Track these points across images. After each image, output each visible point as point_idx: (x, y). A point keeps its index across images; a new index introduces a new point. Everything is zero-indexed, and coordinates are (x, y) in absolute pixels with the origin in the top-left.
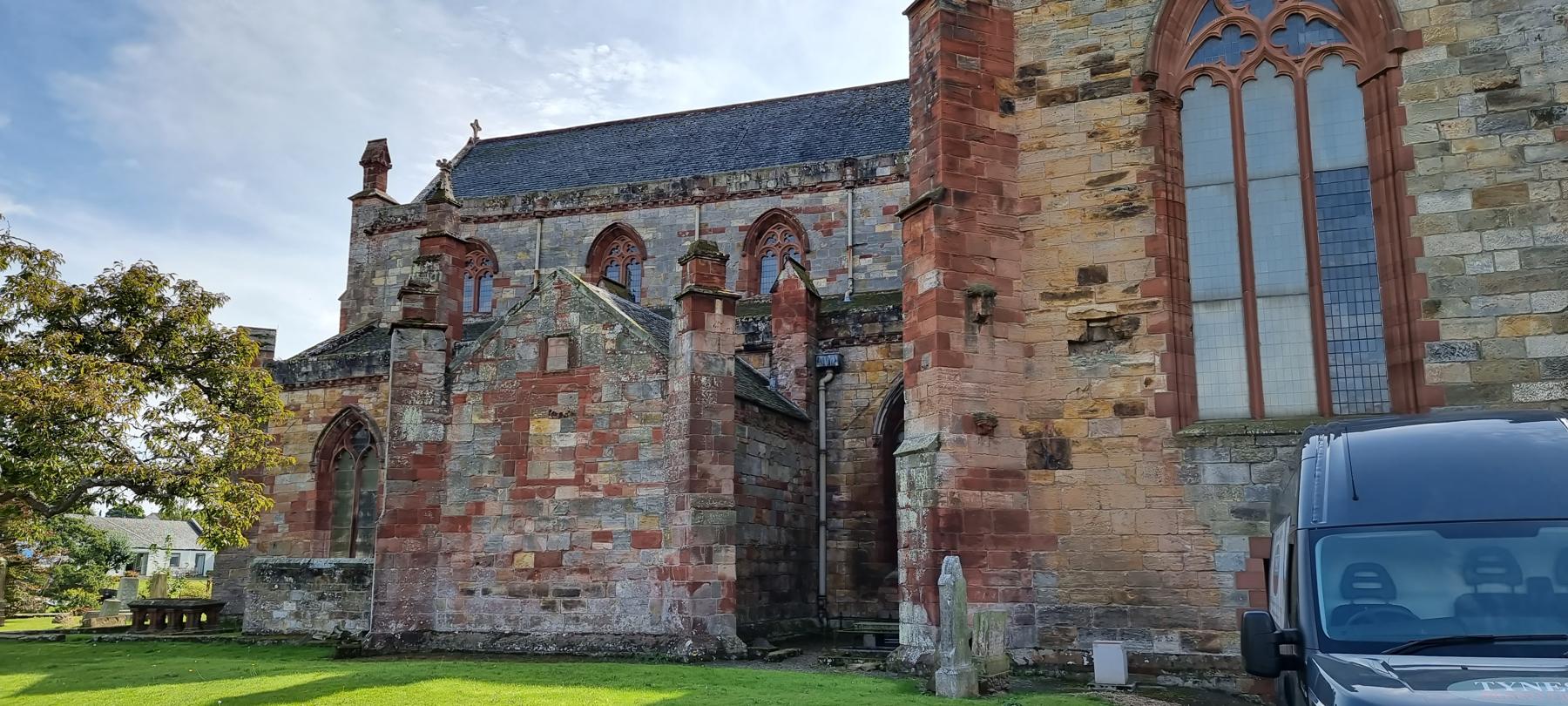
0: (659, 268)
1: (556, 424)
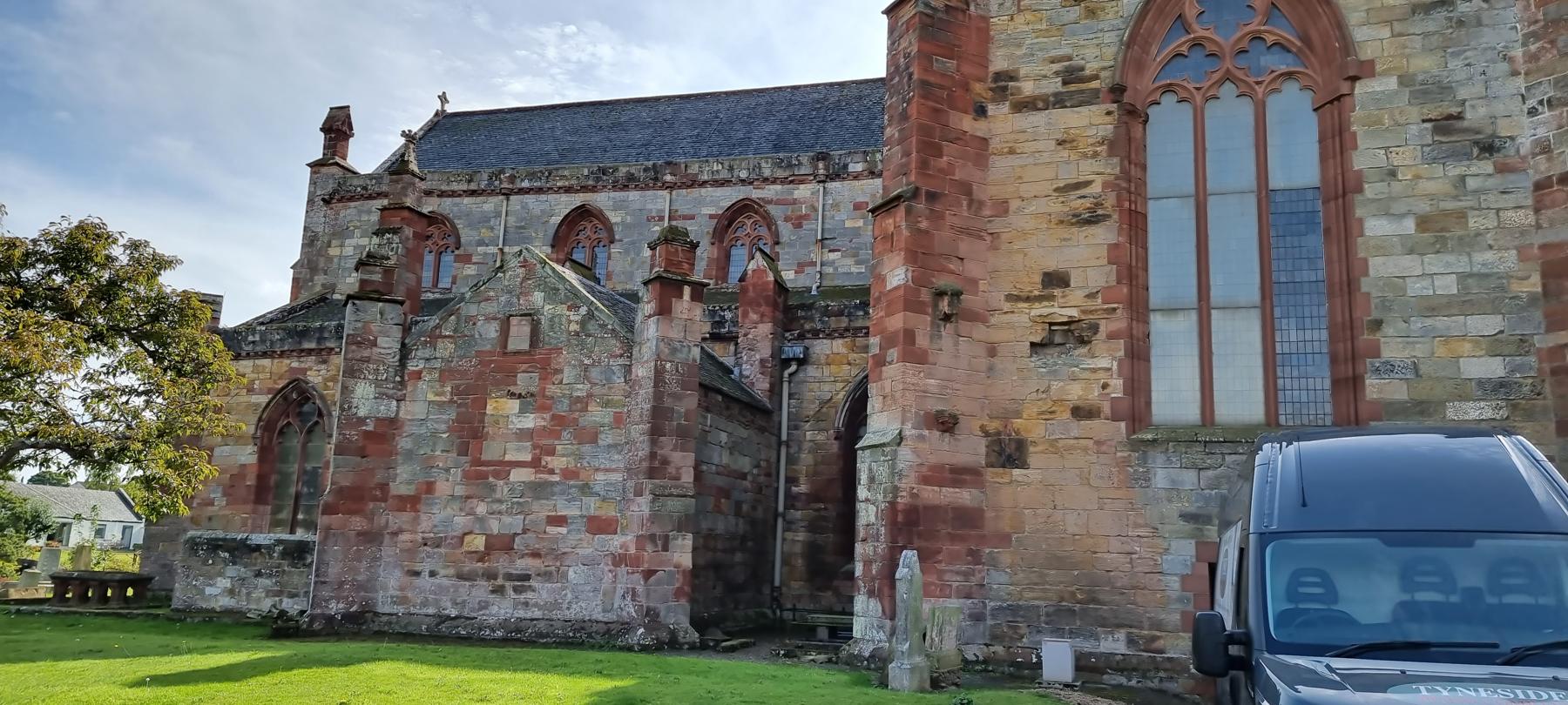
0: (627, 252)
1: (514, 405)
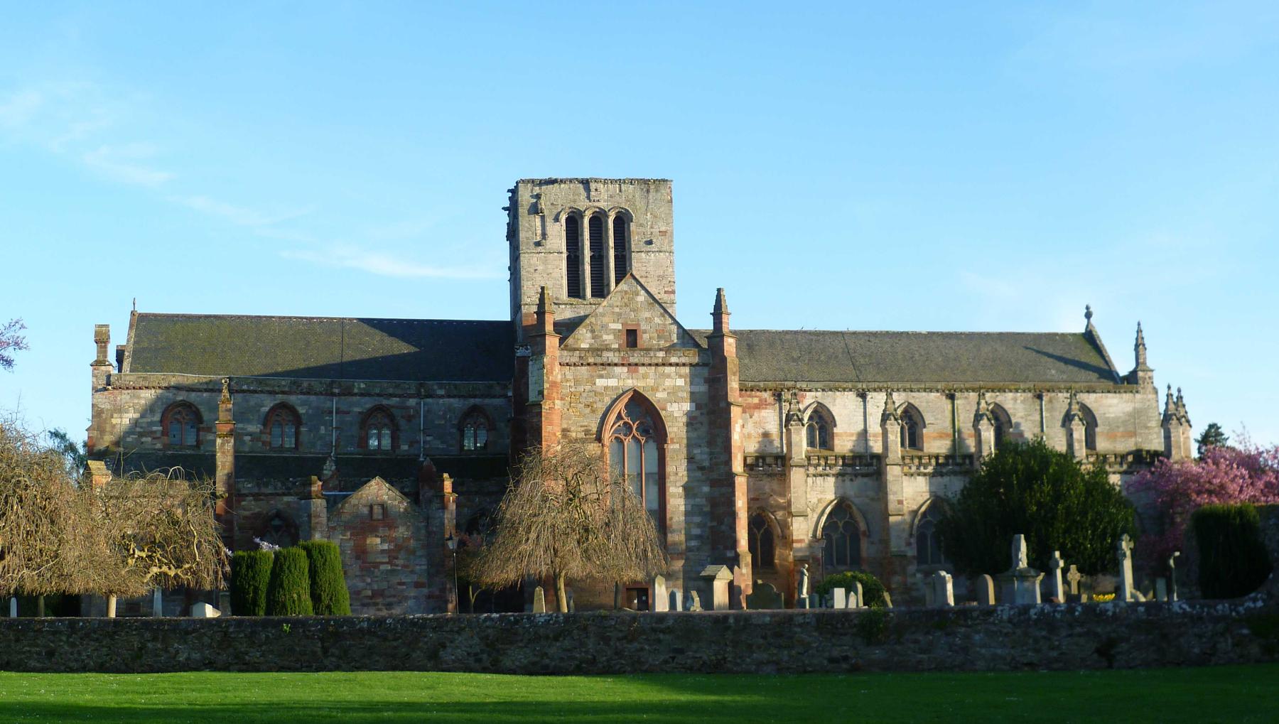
0: (310, 431)
1: (378, 540)
